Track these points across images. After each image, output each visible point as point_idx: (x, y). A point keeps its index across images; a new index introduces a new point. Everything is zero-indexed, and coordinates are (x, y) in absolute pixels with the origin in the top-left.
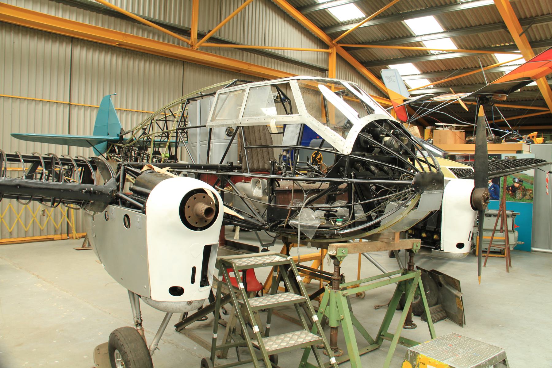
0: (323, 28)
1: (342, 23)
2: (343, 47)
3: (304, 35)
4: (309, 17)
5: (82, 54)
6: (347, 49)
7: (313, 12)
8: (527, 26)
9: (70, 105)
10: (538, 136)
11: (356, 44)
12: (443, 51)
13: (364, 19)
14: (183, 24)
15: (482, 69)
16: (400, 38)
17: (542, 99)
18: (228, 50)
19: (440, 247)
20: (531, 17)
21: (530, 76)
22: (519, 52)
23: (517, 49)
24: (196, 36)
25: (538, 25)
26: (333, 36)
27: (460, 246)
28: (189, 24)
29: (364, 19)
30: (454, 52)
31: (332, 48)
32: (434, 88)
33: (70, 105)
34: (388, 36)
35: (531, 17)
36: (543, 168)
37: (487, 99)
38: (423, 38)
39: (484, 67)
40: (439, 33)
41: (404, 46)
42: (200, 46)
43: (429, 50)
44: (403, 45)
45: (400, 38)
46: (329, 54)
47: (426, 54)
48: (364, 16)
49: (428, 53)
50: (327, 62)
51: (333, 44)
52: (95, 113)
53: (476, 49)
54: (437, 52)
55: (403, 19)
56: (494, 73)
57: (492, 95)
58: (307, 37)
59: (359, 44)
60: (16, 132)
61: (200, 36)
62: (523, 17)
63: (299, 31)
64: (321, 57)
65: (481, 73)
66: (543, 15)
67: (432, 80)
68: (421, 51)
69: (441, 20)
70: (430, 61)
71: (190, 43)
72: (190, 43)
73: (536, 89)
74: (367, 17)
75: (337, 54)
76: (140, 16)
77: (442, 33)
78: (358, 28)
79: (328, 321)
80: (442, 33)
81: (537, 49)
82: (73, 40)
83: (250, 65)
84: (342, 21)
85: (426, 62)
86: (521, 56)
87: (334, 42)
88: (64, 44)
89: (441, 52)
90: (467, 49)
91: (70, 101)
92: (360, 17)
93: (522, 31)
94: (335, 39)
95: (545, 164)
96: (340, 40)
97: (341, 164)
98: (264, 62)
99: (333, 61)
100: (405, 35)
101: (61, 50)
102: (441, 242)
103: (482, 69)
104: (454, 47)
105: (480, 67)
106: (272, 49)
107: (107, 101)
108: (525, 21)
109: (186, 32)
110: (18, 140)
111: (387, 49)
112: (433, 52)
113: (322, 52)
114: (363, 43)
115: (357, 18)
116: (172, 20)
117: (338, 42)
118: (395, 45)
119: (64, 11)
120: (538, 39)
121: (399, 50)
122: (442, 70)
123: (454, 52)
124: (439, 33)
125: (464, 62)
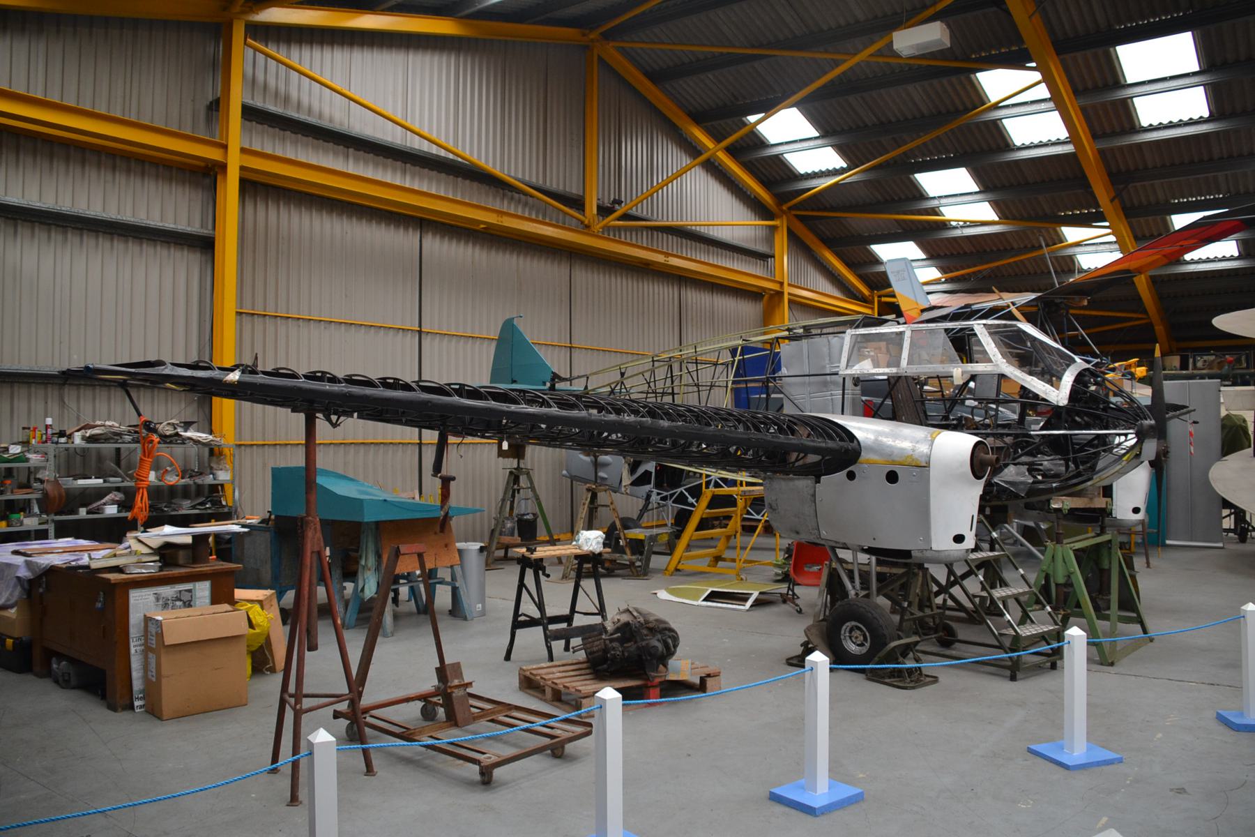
0: (766, 183)
1: (802, 175)
2: (797, 216)
4: (750, 167)
5: (436, 246)
6: (801, 219)
7: (757, 160)
8: (1121, 186)
9: (420, 332)
12: (965, 222)
14: (573, 189)
15: (1045, 250)
16: (900, 200)
22: (1107, 224)
24: (595, 211)
25: (1138, 184)
26: (781, 198)
32: (947, 281)
33: (420, 332)
34: (880, 197)
36: (1186, 417)
37: (1057, 305)
38: (943, 201)
39: (1047, 245)
45: (900, 200)
46: (773, 229)
47: (944, 225)
48: (845, 165)
50: (770, 240)
51: (784, 212)
52: (494, 345)
53: (1030, 219)
56: (1063, 257)
59: (825, 209)
61: (604, 211)
64: (761, 233)
65: (1043, 258)
67: (943, 270)
68: (936, 222)
69: (978, 175)
70: (948, 239)
74: (848, 169)
75: (788, 229)
76: (519, 180)
78: (836, 184)
79: (913, 679)
81: (1133, 220)
82: (424, 223)
83: (667, 255)
84: (802, 172)
86: (1109, 231)
87: (784, 208)
92: (838, 167)
93: (1113, 194)
94: (786, 202)
95: (1189, 412)
97: (1055, 415)
99: (781, 240)
101: (403, 241)
103: (1045, 250)
104: (993, 216)
105: (1041, 247)
107: (509, 328)
109: (577, 203)
112: (954, 224)
114: (833, 209)
116: (554, 184)
117: (790, 208)
118: (891, 213)
119: (413, 176)
120: (1136, 203)
121: (896, 220)
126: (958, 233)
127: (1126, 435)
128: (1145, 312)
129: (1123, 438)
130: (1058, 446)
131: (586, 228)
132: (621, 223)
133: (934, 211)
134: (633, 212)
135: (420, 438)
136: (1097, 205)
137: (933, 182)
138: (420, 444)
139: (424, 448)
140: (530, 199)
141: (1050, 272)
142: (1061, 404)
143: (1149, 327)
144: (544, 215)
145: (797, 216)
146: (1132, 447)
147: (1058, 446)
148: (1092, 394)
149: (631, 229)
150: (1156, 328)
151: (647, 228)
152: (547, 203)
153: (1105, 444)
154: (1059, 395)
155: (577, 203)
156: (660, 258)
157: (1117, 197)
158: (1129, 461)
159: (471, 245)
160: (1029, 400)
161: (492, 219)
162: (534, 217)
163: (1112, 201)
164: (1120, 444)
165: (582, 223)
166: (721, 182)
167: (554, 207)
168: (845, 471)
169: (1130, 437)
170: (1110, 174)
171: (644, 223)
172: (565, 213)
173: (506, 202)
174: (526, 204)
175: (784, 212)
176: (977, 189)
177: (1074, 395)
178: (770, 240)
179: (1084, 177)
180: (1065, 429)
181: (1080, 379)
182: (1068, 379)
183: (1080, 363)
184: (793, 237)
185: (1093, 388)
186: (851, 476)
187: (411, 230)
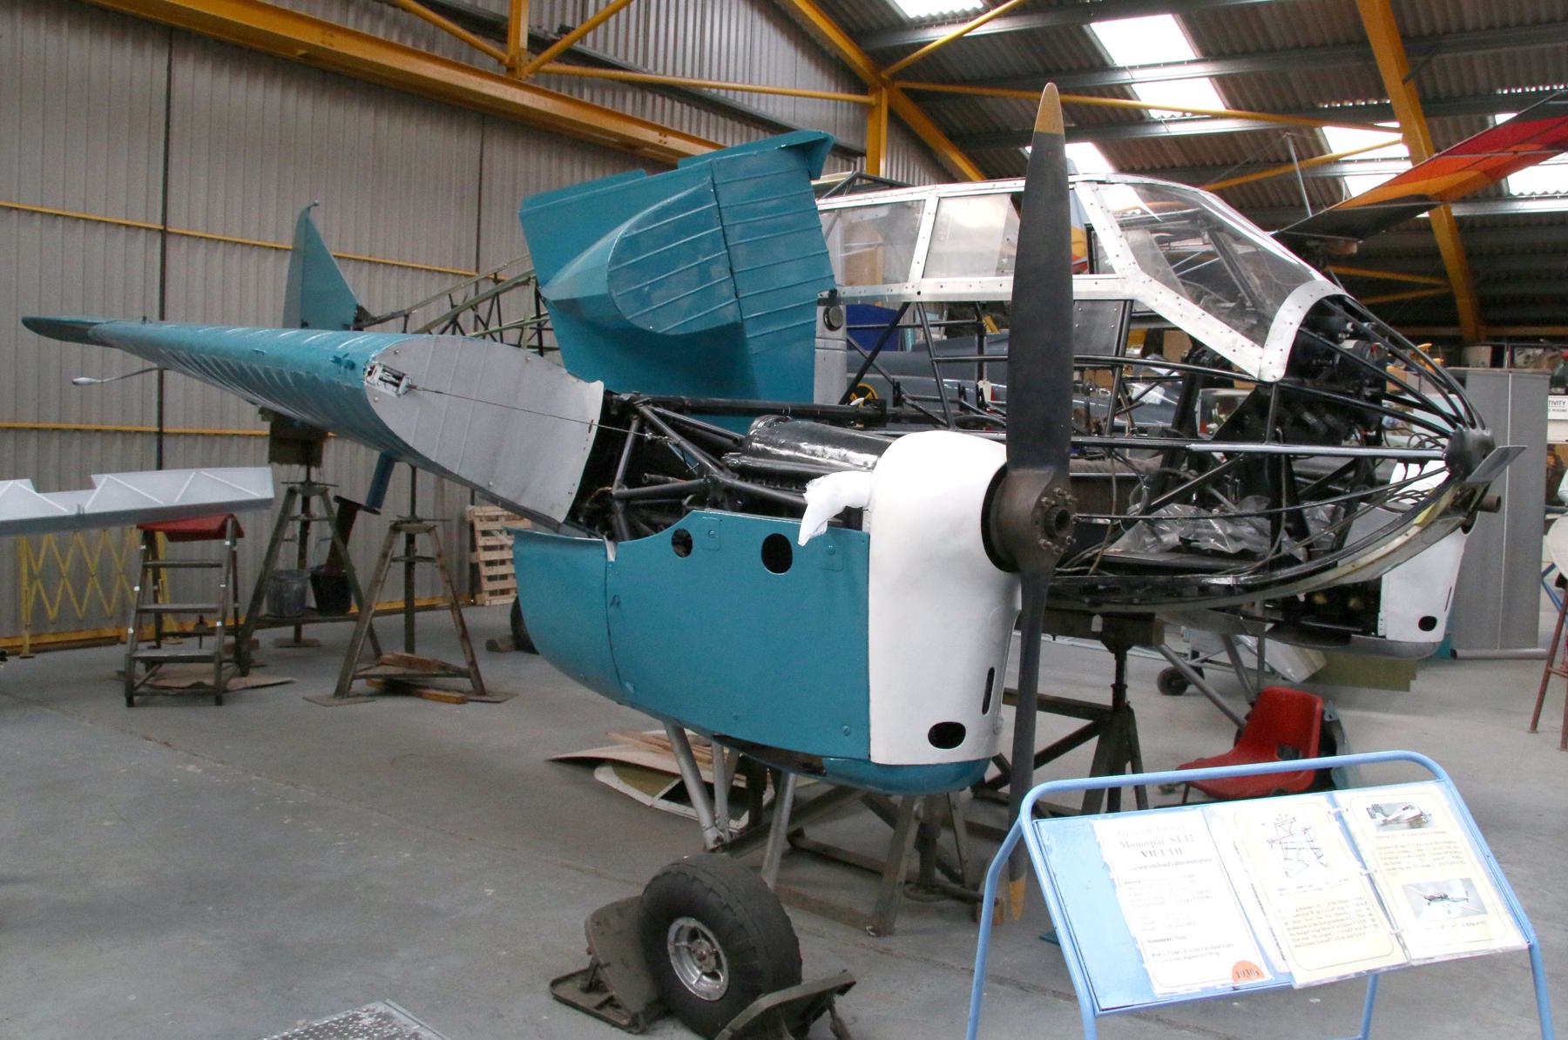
1: (912, 22)
2: (908, 92)
3: (804, 52)
6: (915, 97)
8: (1421, 59)
9: (164, 233)
10: (1432, 353)
11: (943, 82)
12: (1184, 112)
13: (978, 13)
17: (1434, 253)
18: (595, 85)
19: (1375, 629)
20: (1433, 33)
21: (1429, 193)
22: (1396, 125)
23: (1391, 118)
24: (524, 41)
26: (882, 59)
27: (1427, 623)
28: (1430, 126)
29: (978, 13)
30: (1216, 116)
31: (877, 90)
33: (164, 233)
35: (1433, 33)
38: (1137, 74)
40: (1181, 63)
41: (1077, 94)
42: (536, 71)
43: (1147, 108)
44: (1077, 92)
47: (1138, 117)
49: (1142, 117)
52: (287, 261)
54: (1167, 115)
55: (1088, 22)
56: (1324, 180)
57: (1322, 240)
58: (810, 58)
59: (953, 82)
60: (35, 314)
61: (538, 43)
62: (1411, 32)
63: (790, 38)
64: (845, 115)
65: (1293, 181)
66: (1462, 30)
68: (1125, 109)
70: (1145, 140)
71: (507, 60)
72: (507, 60)
73: (1426, 226)
77: (1190, 62)
78: (959, 39)
80: (1190, 62)
85: (1135, 142)
86: (1399, 136)
87: (884, 76)
88: (148, 53)
89: (1178, 115)
90: (1263, 110)
91: (164, 222)
96: (908, 68)
97: (1258, 410)
98: (699, 126)
100: (1075, 67)
102: (1381, 615)
104: (1216, 103)
105: (1290, 160)
106: (718, 88)
107: (305, 227)
108: (1418, 45)
109: (495, 29)
110: (57, 342)
111: (1016, 99)
112: (1155, 114)
113: (855, 103)
114: (964, 82)
115: (957, 10)
122: (1174, 167)
123: (1216, 116)
124: (1181, 63)
125: (1238, 147)
126: (1163, 131)
127: (1422, 461)
128: (1442, 273)
129: (1414, 469)
130: (1257, 477)
131: (510, 74)
132: (563, 68)
133: (1122, 91)
134: (588, 47)
135: (160, 424)
136: (1382, 94)
137: (1120, 38)
138: (160, 434)
139: (167, 442)
140: (404, 17)
141: (1302, 204)
142: (1268, 378)
143: (1448, 301)
144: (431, 44)
145: (908, 92)
146: (1439, 491)
147: (1257, 477)
148: (1345, 356)
149: (581, 81)
150: (1459, 301)
151: (622, 81)
152: (437, 25)
153: (1371, 481)
154: (1266, 360)
155: (495, 29)
156: (652, 136)
157: (1414, 76)
158: (1425, 526)
159: (226, 71)
160: (1204, 369)
161: (314, 38)
162: (395, 39)
163: (1405, 82)
164: (1406, 483)
165: (500, 61)
166: (776, 25)
167: (451, 32)
168: (666, 535)
169: (1432, 466)
170: (1405, 38)
171: (621, 73)
172: (471, 44)
173: (352, 10)
174: (395, 21)
175: (884, 83)
176: (1193, 57)
177: (1301, 358)
178: (859, 128)
179: (1365, 42)
180: (1276, 439)
181: (1318, 317)
182: (1288, 319)
183: (1320, 286)
184: (894, 118)
185: (1349, 344)
186: (683, 543)
187: (148, 53)
